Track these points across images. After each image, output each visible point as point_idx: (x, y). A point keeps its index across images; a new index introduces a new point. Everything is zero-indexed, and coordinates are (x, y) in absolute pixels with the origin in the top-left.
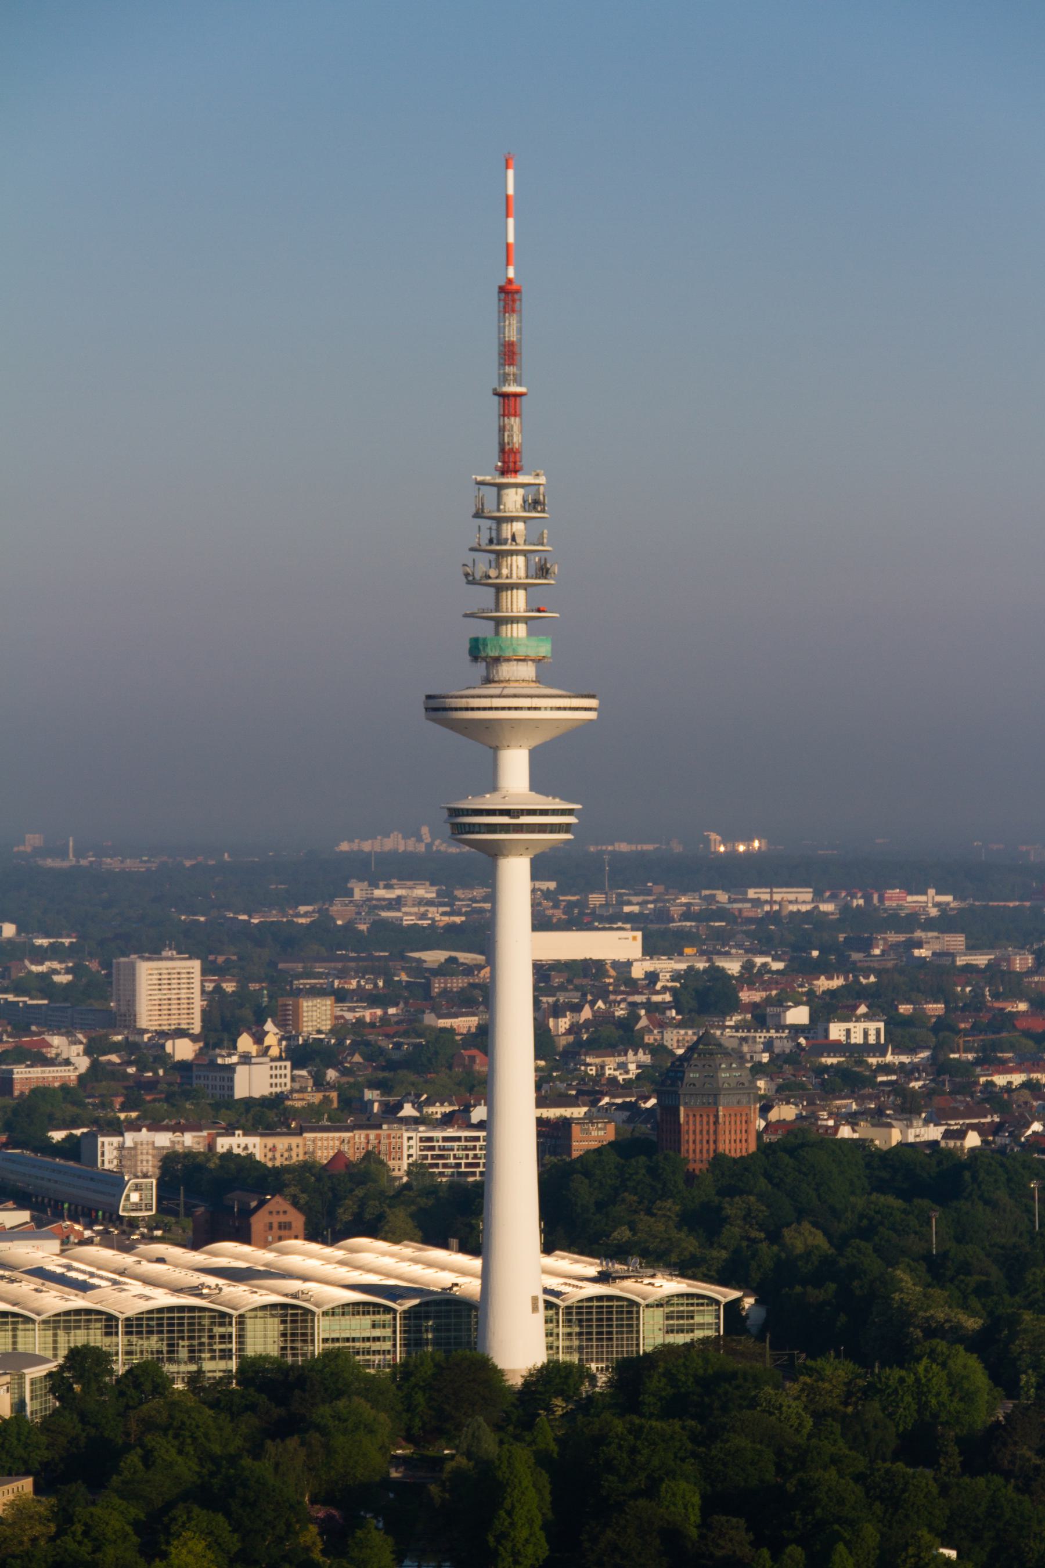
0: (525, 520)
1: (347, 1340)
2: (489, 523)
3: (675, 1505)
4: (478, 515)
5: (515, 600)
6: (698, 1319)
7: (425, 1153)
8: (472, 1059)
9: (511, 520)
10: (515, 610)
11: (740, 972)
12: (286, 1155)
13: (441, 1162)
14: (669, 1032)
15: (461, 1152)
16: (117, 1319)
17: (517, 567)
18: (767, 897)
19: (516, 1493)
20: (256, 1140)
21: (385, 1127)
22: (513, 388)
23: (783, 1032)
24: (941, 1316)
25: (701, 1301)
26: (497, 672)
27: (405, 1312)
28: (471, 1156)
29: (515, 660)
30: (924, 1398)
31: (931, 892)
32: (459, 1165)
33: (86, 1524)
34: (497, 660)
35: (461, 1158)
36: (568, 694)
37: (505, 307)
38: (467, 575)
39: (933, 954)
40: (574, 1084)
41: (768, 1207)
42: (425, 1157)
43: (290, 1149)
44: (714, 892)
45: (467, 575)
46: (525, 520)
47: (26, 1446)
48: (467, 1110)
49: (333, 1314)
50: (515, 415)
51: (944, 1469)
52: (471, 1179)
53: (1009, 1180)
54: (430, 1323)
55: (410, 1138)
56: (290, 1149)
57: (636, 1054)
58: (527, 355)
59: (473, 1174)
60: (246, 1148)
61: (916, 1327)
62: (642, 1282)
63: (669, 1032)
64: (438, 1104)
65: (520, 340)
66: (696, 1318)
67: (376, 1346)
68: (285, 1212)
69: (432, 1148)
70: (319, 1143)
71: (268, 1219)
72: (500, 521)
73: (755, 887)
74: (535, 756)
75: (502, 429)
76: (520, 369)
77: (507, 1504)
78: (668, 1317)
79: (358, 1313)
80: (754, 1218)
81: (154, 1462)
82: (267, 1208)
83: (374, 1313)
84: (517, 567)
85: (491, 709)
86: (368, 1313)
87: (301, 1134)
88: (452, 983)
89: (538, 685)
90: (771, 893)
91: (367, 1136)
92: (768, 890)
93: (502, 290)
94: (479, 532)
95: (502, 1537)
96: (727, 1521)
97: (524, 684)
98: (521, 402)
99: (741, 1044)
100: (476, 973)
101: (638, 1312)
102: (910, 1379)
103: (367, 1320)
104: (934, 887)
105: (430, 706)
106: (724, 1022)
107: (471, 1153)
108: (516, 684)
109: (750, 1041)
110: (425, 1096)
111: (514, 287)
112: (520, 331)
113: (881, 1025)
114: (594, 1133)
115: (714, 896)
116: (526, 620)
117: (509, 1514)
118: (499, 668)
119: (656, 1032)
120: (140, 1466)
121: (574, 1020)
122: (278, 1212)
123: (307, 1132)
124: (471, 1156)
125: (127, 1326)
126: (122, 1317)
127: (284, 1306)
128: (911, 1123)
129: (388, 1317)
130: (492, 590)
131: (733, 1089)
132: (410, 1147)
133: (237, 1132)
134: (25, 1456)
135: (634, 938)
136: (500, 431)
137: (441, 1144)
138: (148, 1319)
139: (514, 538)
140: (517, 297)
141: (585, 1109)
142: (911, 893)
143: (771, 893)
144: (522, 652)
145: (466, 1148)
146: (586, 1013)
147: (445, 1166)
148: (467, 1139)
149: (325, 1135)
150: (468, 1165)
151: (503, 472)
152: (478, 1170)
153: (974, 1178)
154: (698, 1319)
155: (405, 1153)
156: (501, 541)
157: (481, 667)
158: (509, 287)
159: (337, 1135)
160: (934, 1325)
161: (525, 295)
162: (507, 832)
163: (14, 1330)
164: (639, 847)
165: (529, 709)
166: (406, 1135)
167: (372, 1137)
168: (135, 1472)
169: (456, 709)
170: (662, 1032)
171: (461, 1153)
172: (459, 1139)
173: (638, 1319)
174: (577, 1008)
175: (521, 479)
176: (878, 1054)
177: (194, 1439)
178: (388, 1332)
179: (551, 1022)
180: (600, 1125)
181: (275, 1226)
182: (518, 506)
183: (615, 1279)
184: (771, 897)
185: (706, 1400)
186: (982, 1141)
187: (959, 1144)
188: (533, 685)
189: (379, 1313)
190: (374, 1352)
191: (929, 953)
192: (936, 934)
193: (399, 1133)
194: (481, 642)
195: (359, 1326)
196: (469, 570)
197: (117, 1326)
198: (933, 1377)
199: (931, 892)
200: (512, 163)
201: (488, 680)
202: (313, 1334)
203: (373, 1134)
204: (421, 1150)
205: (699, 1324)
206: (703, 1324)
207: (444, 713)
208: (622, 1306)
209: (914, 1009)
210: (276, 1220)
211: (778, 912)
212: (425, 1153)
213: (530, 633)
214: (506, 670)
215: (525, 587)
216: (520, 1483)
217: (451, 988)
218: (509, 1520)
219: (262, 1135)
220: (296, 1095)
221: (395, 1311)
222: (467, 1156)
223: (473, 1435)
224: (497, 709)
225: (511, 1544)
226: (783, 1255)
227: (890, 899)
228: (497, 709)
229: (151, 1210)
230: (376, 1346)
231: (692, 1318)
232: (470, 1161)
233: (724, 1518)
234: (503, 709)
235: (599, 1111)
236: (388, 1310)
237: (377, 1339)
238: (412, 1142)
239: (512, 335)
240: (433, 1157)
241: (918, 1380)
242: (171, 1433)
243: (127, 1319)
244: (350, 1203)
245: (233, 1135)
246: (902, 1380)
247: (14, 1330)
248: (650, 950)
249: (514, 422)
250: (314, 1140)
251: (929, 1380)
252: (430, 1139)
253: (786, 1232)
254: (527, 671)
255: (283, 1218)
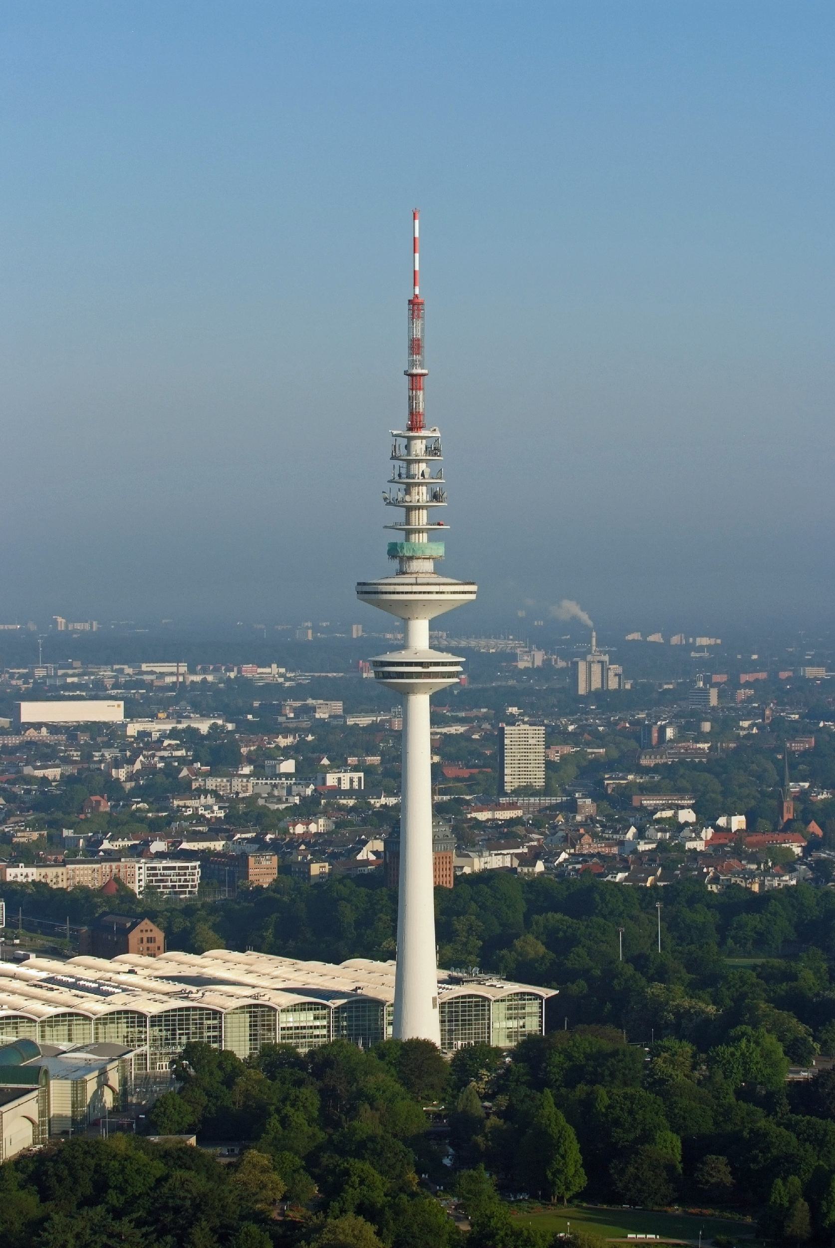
0: (426, 461)
1: (297, 1028)
2: (401, 463)
3: (666, 1147)
4: (393, 458)
5: (421, 517)
6: (528, 1010)
7: (151, 878)
8: (98, 802)
9: (419, 461)
10: (421, 524)
11: (208, 731)
12: (54, 880)
13: (162, 884)
14: (236, 780)
15: (175, 877)
16: (145, 1016)
17: (421, 495)
18: (174, 669)
19: (567, 1143)
20: (34, 870)
21: (123, 860)
22: (418, 371)
23: (291, 780)
24: (686, 1004)
25: (530, 997)
26: (409, 566)
27: (335, 1008)
28: (182, 880)
29: (424, 558)
30: (748, 1066)
31: (274, 666)
32: (174, 887)
33: (359, 1176)
34: (411, 558)
35: (176, 882)
36: (460, 582)
37: (413, 315)
38: (385, 499)
39: (330, 717)
40: (194, 822)
41: (484, 923)
42: (151, 881)
43: (57, 876)
44: (122, 666)
45: (385, 499)
46: (426, 461)
47: (179, 1113)
48: (147, 844)
49: (288, 1011)
50: (420, 389)
51: (780, 1115)
52: (182, 896)
53: (625, 900)
54: (345, 1015)
55: (140, 868)
56: (57, 876)
57: (206, 798)
58: (427, 346)
59: (185, 893)
60: (27, 876)
61: (669, 1012)
62: (484, 984)
63: (236, 780)
64: (120, 840)
65: (423, 336)
66: (526, 1008)
67: (317, 1032)
68: (151, 931)
69: (155, 875)
70: (77, 872)
71: (140, 935)
72: (409, 462)
73: (146, 663)
74: (434, 625)
75: (411, 399)
76: (423, 357)
77: (562, 1151)
78: (509, 1009)
79: (305, 1010)
80: (475, 931)
81: (289, 1125)
82: (139, 927)
83: (315, 1010)
84: (421, 495)
85: (411, 593)
86: (311, 1009)
87: (64, 866)
88: (8, 740)
89: (436, 576)
90: (178, 666)
91: (111, 866)
92: (176, 664)
93: (410, 302)
94: (391, 468)
95: (559, 1171)
96: (717, 1159)
97: (428, 575)
98: (424, 380)
99: (273, 790)
100: (23, 733)
101: (489, 1006)
102: (738, 1054)
103: (310, 1015)
104: (276, 663)
105: (360, 590)
106: (237, 771)
107: (183, 878)
108: (423, 575)
109: (279, 787)
110: (110, 834)
111: (420, 300)
112: (423, 330)
113: (362, 775)
114: (264, 863)
115: (123, 669)
116: (428, 530)
117: (563, 1157)
118: (411, 564)
119: (200, 780)
120: (280, 1128)
121: (129, 770)
122: (147, 931)
123: (69, 864)
124: (182, 880)
125: (152, 1021)
126: (149, 1015)
127: (250, 1006)
128: (482, 854)
129: (325, 1012)
130: (404, 509)
131: (441, 840)
132: (140, 874)
133: (21, 865)
134: (180, 1120)
135: (119, 706)
136: (409, 399)
137: (161, 871)
138: (166, 1016)
139: (423, 475)
140: (420, 307)
141: (223, 842)
142: (259, 667)
143: (178, 666)
144: (428, 553)
145: (179, 875)
146: (138, 766)
147: (165, 887)
148: (180, 868)
149: (82, 866)
150: (180, 886)
151: (411, 429)
152: (187, 890)
153: (603, 899)
154: (528, 1010)
155: (137, 879)
156: (409, 476)
157: (395, 564)
158: (416, 301)
159: (90, 866)
160: (682, 1011)
161: (427, 307)
162: (411, 678)
163: (70, 1025)
164: (6, 627)
165: (437, 593)
166: (137, 865)
167: (114, 867)
168: (277, 1132)
169: (386, 593)
170: (205, 780)
171: (175, 878)
172: (174, 868)
173: (489, 1010)
174: (131, 762)
175: (423, 433)
176: (375, 797)
177: (304, 1107)
178: (325, 1023)
179: (114, 772)
180: (267, 857)
181: (145, 940)
182: (423, 452)
183: (463, 982)
184: (178, 669)
185: (599, 1070)
186: (545, 868)
187: (531, 870)
188: (433, 575)
189: (318, 1009)
190: (315, 1036)
191: (326, 716)
192: (321, 701)
193: (133, 864)
194: (399, 545)
195: (306, 1018)
196: (386, 495)
197: (146, 1022)
198: (753, 1051)
199: (274, 666)
200: (417, 216)
201: (402, 572)
202: (275, 1025)
203: (114, 865)
204: (148, 877)
205: (528, 1013)
206: (532, 1013)
207: (377, 595)
208: (479, 1002)
209: (359, 761)
210: (145, 936)
211: (184, 682)
212: (151, 878)
213: (429, 540)
214: (415, 565)
215: (426, 507)
216: (569, 1136)
217: (8, 743)
218: (563, 1161)
219: (37, 867)
220: (19, 834)
221: (329, 1007)
222: (180, 881)
223: (467, 1099)
224: (415, 593)
225: (564, 1177)
226: (520, 958)
227: (246, 671)
228: (415, 593)
229: (2, 924)
230: (317, 1032)
231: (524, 1008)
232: (182, 883)
233: (714, 1157)
234: (420, 593)
235: (233, 844)
236: (325, 1007)
237: (317, 1027)
238: (142, 871)
239: (418, 334)
240: (157, 881)
241: (743, 1054)
242: (288, 1103)
243: (152, 1017)
244: (161, 920)
245: (18, 866)
246: (733, 1054)
247: (70, 1025)
248: (131, 713)
249: (420, 394)
250: (73, 870)
251: (751, 1054)
252: (154, 868)
253: (516, 942)
254: (429, 566)
255: (149, 935)
